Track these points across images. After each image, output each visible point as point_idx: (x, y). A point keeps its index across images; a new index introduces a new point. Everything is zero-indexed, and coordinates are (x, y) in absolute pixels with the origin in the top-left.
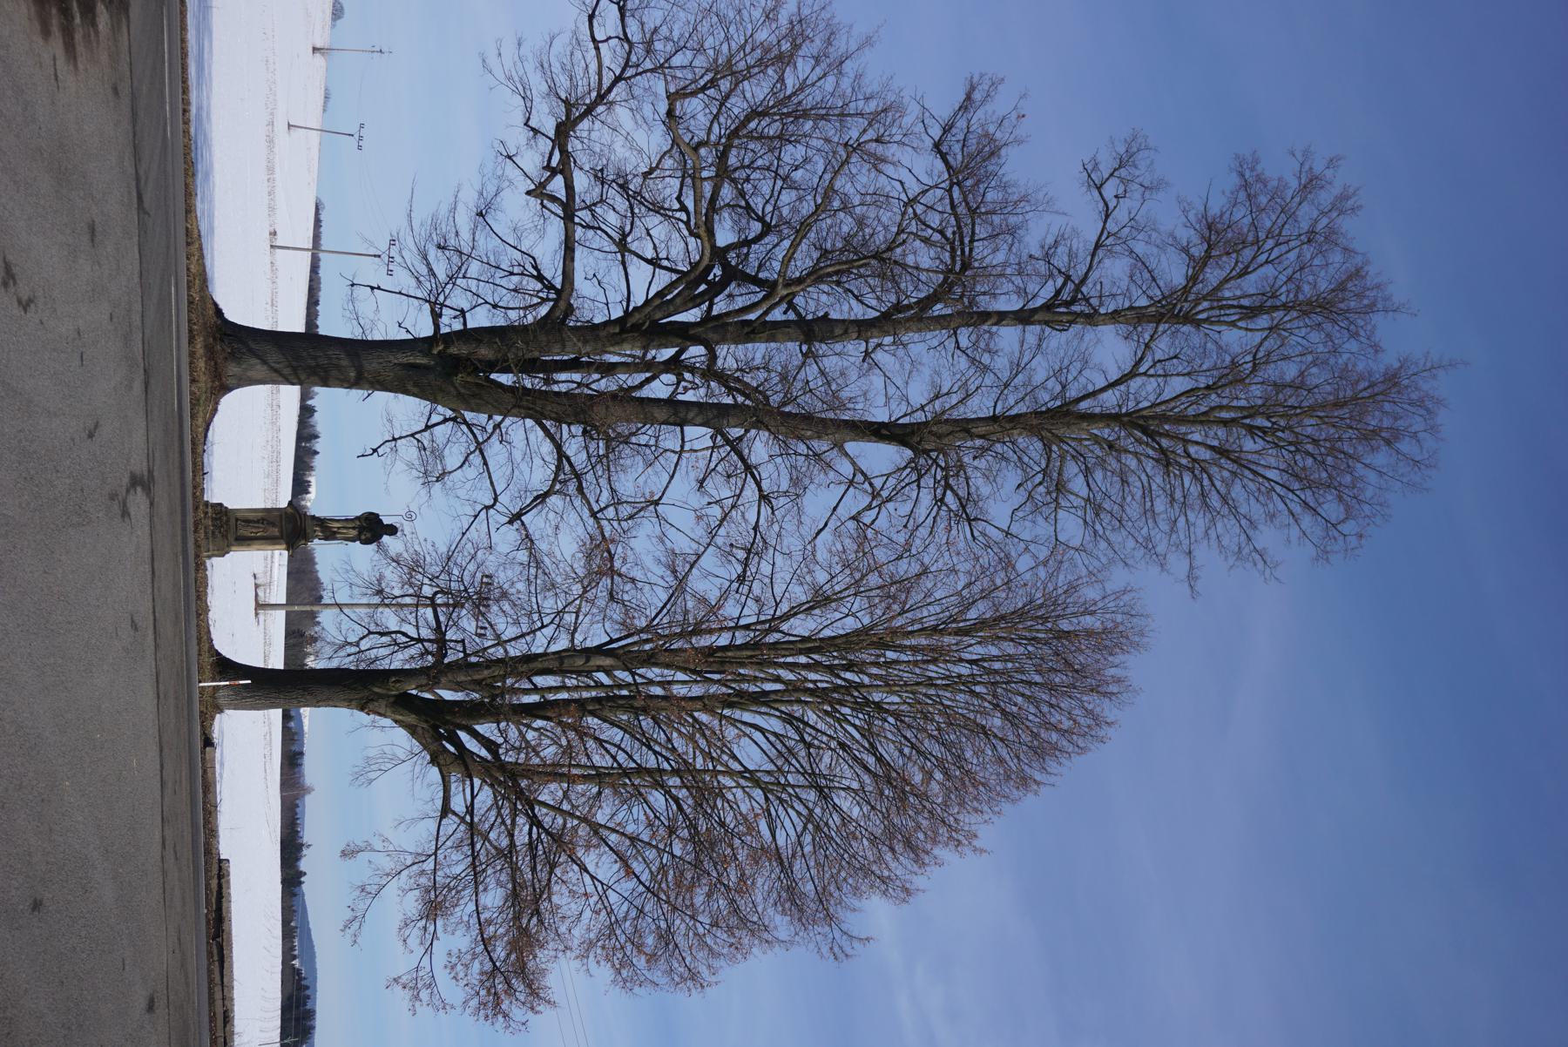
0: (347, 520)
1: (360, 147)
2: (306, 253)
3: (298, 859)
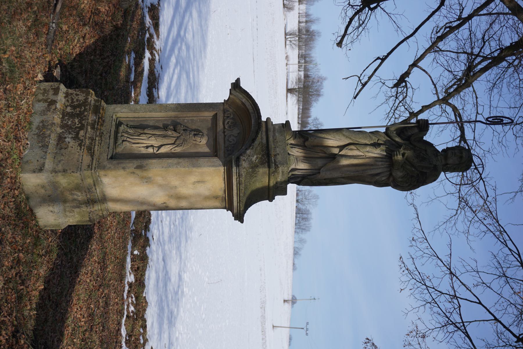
1: (307, 334)
2: (287, 329)
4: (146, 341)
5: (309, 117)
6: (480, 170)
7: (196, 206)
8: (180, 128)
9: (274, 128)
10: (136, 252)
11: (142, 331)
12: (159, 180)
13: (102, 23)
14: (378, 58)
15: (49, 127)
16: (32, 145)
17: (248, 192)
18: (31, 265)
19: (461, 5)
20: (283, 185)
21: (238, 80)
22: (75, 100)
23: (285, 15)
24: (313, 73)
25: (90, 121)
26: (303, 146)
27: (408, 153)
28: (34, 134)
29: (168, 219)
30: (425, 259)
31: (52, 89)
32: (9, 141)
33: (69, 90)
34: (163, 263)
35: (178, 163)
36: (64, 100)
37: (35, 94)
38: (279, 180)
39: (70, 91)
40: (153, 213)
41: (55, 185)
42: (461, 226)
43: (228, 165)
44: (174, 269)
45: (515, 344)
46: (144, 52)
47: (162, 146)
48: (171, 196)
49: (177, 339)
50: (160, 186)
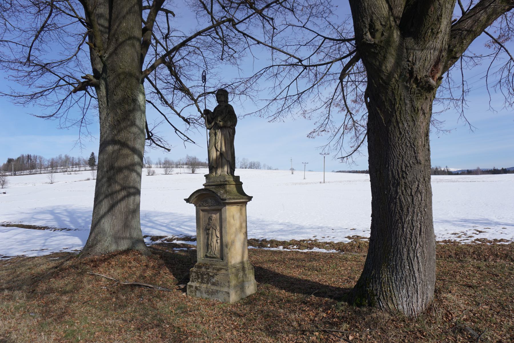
1: (308, 163)
3: (498, 170)
4: (310, 240)
5: (206, 163)
6: (227, 85)
7: (245, 219)
8: (208, 227)
10: (269, 246)
11: (305, 242)
12: (232, 237)
13: (159, 264)
14: (176, 132)
16: (217, 298)
17: (238, 194)
18: (273, 296)
19: (151, 93)
20: (235, 178)
21: (185, 200)
23: (157, 174)
24: (185, 161)
25: (205, 270)
26: (216, 168)
27: (219, 119)
29: (253, 230)
30: (269, 111)
32: (215, 309)
35: (225, 228)
36: (195, 283)
37: (192, 297)
38: (232, 180)
39: (191, 280)
40: (249, 238)
41: (236, 286)
42: (255, 94)
43: (225, 204)
44: (277, 227)
45: (308, 70)
46: (173, 243)
47: (216, 236)
48: (241, 231)
49: (309, 225)
50: (235, 236)
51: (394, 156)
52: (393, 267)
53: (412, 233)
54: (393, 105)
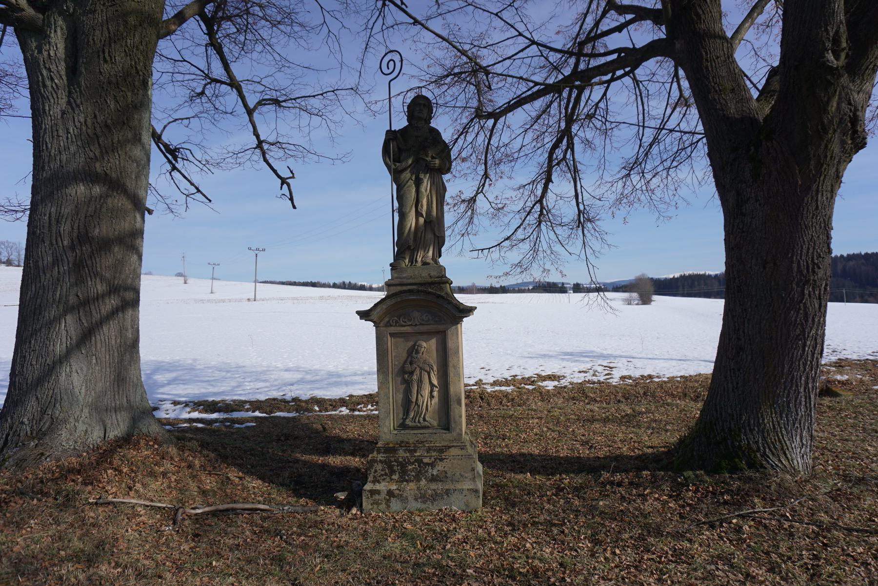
0: (401, 198)
8: (408, 367)
9: (397, 278)
15: (423, 492)
21: (358, 313)
22: (383, 473)
28: (433, 505)
31: (371, 497)
33: (369, 480)
34: (295, 385)
44: (289, 376)
51: (804, 241)
52: (783, 405)
53: (814, 353)
54: (819, 164)
